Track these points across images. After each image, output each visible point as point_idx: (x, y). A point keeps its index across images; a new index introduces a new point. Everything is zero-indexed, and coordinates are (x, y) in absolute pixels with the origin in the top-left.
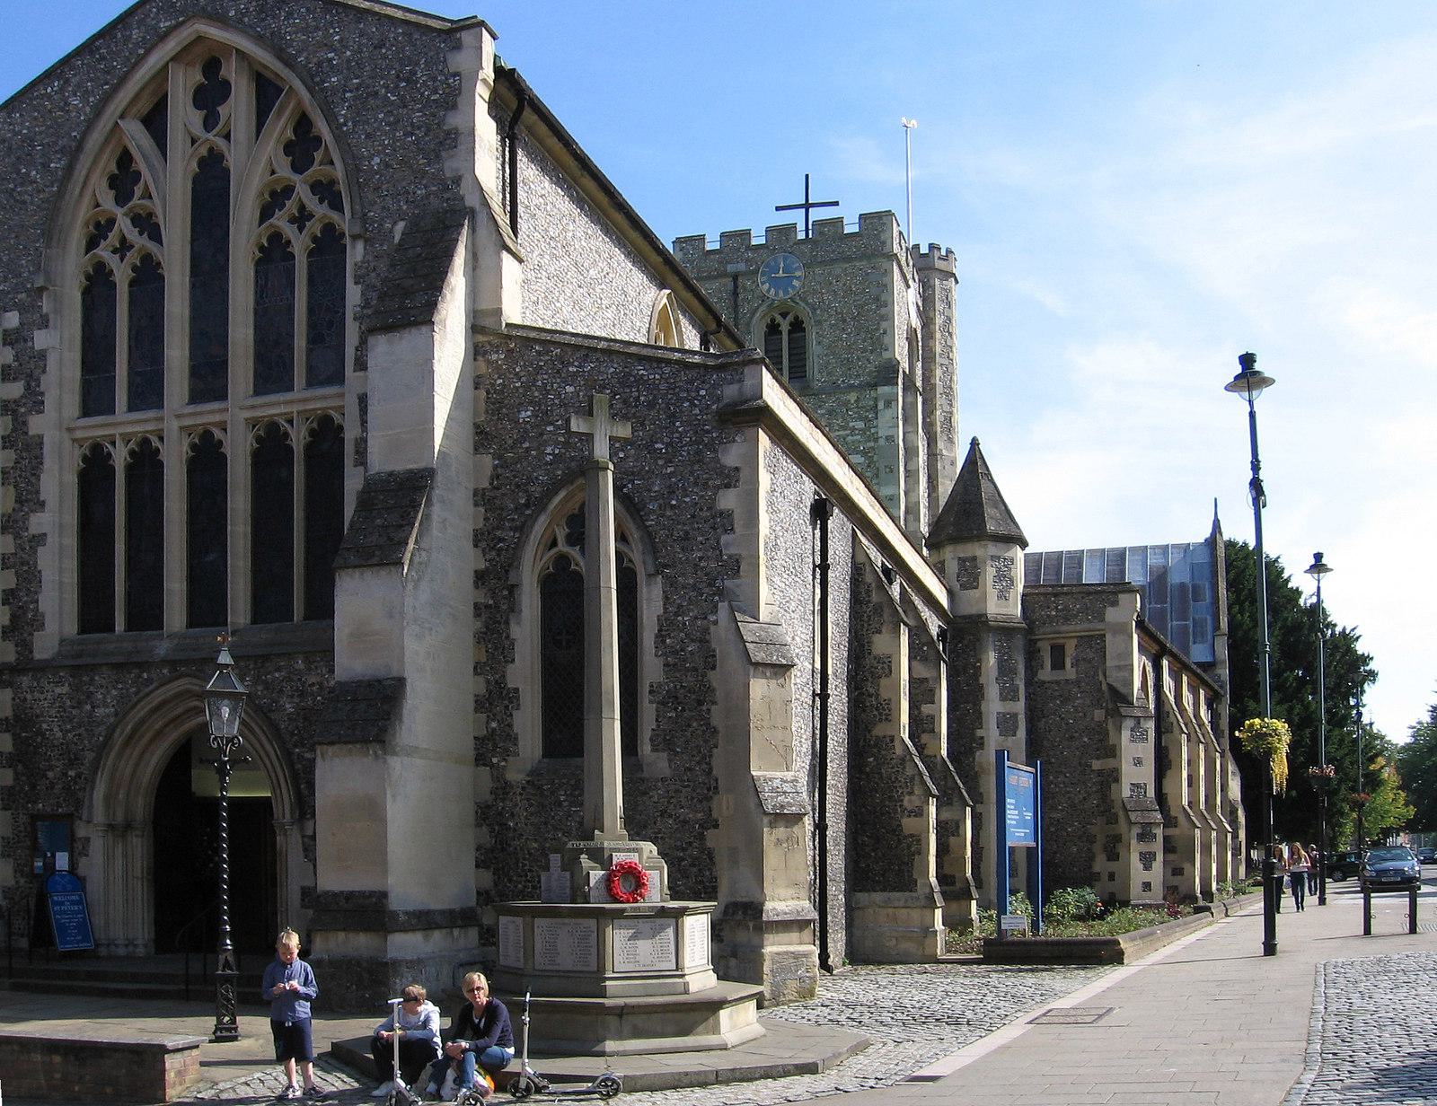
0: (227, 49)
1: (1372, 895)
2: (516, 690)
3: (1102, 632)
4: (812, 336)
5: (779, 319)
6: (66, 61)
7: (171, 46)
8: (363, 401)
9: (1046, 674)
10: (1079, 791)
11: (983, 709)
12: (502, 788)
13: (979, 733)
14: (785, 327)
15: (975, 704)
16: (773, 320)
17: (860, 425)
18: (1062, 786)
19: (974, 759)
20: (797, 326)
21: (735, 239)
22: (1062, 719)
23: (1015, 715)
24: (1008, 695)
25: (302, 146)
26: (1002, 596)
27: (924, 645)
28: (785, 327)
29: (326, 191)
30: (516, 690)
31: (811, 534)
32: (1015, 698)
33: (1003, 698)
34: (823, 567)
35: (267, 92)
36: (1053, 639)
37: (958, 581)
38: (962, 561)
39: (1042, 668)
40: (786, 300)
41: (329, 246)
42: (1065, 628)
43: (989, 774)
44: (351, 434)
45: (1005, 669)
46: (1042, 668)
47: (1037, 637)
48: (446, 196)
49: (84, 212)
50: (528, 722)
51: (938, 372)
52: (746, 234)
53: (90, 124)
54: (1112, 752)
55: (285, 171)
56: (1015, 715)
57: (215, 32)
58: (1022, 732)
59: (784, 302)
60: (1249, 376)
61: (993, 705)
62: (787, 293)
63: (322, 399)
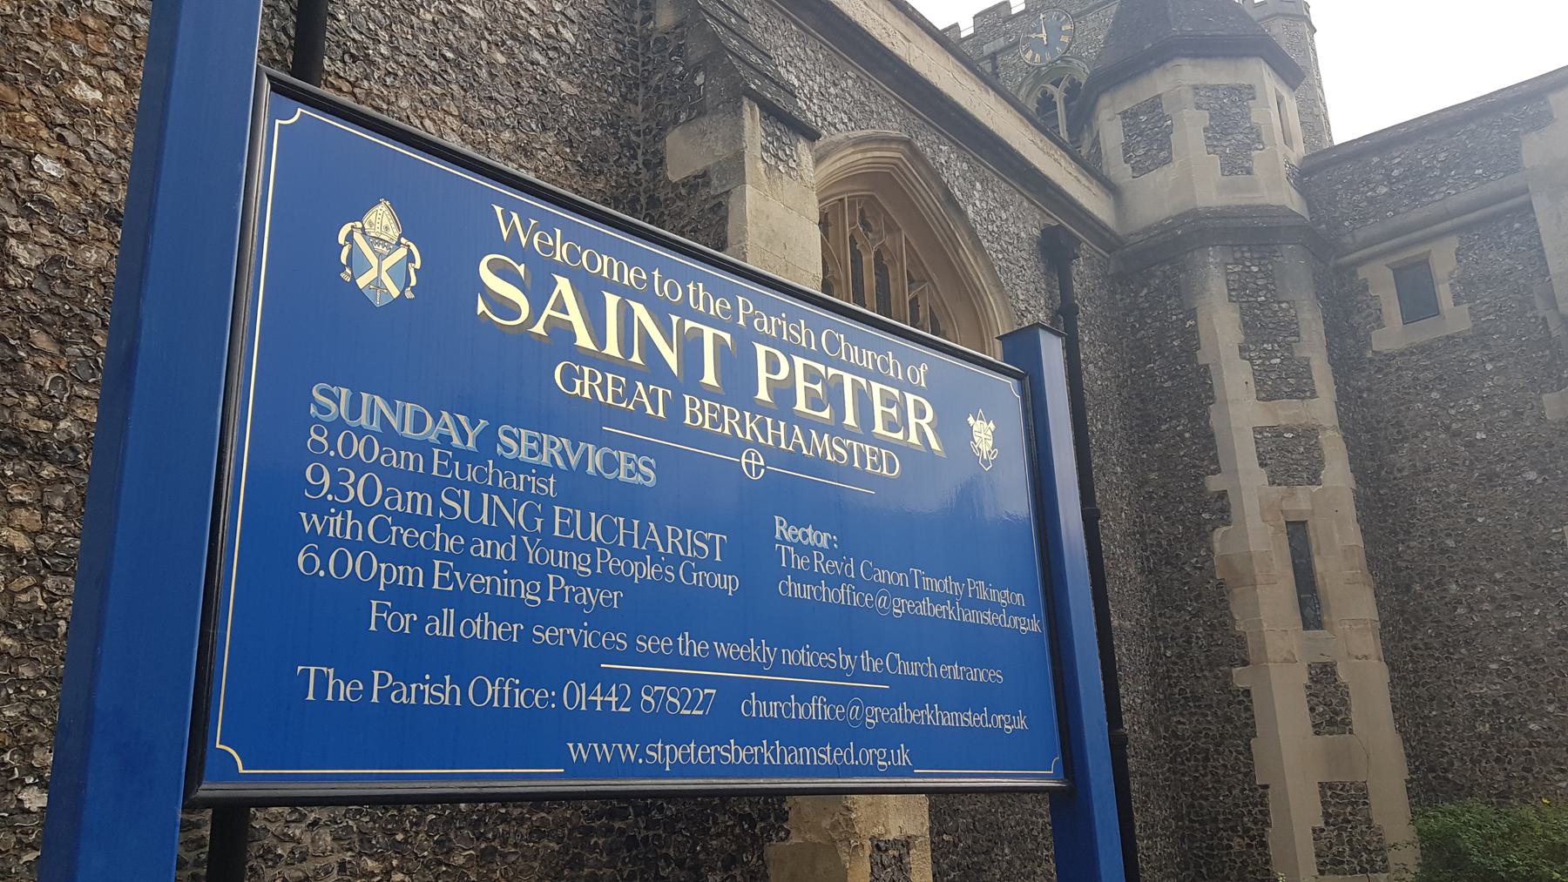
1: (452, 611)
2: (1247, 692)
3: (1522, 199)
5: (1051, 88)
10: (1542, 617)
11: (1215, 422)
13: (1214, 484)
16: (1044, 93)
18: (1486, 606)
19: (1210, 550)
22: (1456, 434)
23: (1309, 434)
30: (1247, 692)
32: (1303, 390)
33: (1267, 393)
36: (1393, 251)
38: (1129, 116)
39: (1381, 326)
43: (1254, 585)
46: (1381, 326)
56: (1309, 434)
58: (1338, 473)
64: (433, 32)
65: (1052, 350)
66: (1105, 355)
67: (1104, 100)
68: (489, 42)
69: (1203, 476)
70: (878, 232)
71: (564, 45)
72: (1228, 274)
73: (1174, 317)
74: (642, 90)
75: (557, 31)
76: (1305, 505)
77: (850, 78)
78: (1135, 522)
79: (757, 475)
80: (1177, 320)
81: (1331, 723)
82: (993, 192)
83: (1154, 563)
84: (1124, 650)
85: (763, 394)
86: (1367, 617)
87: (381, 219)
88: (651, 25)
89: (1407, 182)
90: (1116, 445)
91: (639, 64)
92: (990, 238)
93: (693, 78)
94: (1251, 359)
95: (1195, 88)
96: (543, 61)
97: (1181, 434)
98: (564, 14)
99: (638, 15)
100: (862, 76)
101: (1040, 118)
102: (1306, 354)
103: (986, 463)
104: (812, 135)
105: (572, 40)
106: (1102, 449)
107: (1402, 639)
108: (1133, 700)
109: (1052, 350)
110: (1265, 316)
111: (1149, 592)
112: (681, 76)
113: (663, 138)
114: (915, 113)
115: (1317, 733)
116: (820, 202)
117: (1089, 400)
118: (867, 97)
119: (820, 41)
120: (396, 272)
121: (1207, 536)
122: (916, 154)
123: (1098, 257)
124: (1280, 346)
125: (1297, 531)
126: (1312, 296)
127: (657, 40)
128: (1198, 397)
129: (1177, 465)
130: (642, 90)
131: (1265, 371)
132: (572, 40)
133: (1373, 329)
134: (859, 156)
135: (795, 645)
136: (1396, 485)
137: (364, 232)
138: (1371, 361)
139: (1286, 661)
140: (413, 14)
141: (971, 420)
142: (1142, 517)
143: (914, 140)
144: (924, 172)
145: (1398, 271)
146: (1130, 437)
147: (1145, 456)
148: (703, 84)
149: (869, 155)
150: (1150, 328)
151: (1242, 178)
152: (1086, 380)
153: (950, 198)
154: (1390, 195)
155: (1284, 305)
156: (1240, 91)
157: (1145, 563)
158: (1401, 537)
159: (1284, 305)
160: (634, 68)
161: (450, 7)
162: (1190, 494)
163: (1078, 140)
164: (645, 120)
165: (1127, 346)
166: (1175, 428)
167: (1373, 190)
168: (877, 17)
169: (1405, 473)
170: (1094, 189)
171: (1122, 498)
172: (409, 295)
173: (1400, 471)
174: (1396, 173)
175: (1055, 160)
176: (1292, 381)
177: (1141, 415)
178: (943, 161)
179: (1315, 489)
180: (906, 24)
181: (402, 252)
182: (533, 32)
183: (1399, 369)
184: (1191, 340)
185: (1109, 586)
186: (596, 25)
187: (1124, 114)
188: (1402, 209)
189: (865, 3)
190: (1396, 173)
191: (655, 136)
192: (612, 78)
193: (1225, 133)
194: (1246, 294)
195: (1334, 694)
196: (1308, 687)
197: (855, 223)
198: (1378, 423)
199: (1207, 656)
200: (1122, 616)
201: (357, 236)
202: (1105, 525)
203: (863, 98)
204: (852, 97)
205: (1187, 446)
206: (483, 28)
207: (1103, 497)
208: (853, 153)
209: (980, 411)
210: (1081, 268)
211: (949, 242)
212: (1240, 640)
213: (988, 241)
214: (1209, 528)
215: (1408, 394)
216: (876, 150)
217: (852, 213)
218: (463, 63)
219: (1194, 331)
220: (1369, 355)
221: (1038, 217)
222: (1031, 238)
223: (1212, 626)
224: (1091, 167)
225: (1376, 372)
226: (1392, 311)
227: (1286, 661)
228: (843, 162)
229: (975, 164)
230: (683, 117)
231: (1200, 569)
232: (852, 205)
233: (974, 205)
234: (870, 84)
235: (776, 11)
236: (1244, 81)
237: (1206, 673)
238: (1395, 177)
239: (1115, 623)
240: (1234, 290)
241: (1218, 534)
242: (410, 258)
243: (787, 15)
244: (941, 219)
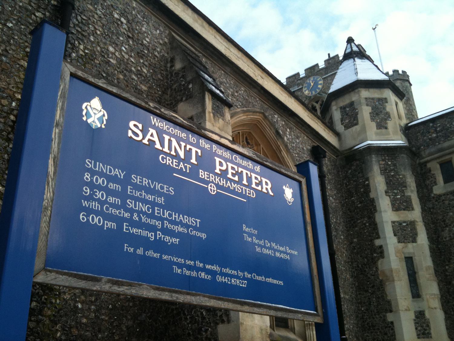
2: (392, 323)
5: (315, 104)
11: (377, 220)
13: (377, 242)
15: (369, 218)
19: (377, 268)
26: (382, 125)
27: (189, 83)
30: (392, 323)
32: (409, 207)
33: (396, 207)
37: (342, 124)
40: (316, 95)
42: (446, 144)
43: (393, 281)
47: (426, 159)
48: (177, 90)
52: (298, 74)
56: (412, 224)
58: (423, 238)
59: (315, 96)
62: (316, 91)
64: (99, 67)
65: (314, 170)
66: (336, 194)
67: (333, 103)
68: (118, 71)
69: (374, 240)
70: (252, 145)
71: (143, 73)
72: (380, 165)
73: (361, 181)
74: (170, 90)
75: (141, 69)
76: (411, 251)
77: (242, 90)
78: (349, 258)
79: (214, 192)
80: (362, 181)
81: (423, 334)
82: (294, 133)
83: (357, 274)
84: (346, 307)
85: (217, 171)
86: (436, 293)
87: (96, 103)
88: (174, 68)
89: (443, 133)
90: (341, 228)
91: (169, 81)
92: (293, 149)
93: (188, 85)
94: (389, 196)
95: (366, 98)
96: (136, 79)
97: (365, 224)
98: (143, 64)
99: (169, 65)
100: (247, 90)
101: (312, 110)
102: (409, 194)
103: (290, 202)
104: (229, 106)
105: (146, 72)
106: (336, 229)
107: (448, 302)
108: (350, 326)
109: (314, 170)
110: (394, 180)
111: (355, 285)
112: (184, 85)
113: (177, 106)
114: (265, 103)
115: (419, 338)
116: (232, 132)
117: (330, 210)
118: (248, 97)
119: (232, 77)
120: (100, 119)
121: (376, 263)
122: (265, 117)
123: (332, 158)
124: (400, 191)
125: (409, 261)
126: (411, 173)
127: (175, 73)
128: (371, 210)
129: (364, 236)
130: (170, 90)
131: (395, 200)
132: (146, 72)
133: (433, 186)
134: (245, 117)
135: (226, 268)
136: (444, 244)
137: (90, 106)
138: (433, 198)
139: (406, 310)
140: (93, 61)
141: (284, 187)
142: (351, 256)
143: (265, 113)
144: (269, 124)
145: (442, 165)
146: (346, 225)
147: (352, 232)
148: (192, 88)
149: (249, 117)
150: (352, 184)
151: (384, 130)
152: (329, 202)
153: (277, 133)
154: (437, 137)
155: (401, 176)
156: (382, 100)
157: (353, 274)
158: (447, 263)
159: (401, 176)
160: (167, 82)
161: (105, 59)
162: (369, 247)
163: (324, 118)
164: (170, 100)
165: (344, 191)
166: (363, 222)
167: (431, 135)
168: (252, 70)
169: (448, 239)
170: (331, 134)
171: (344, 248)
172: (103, 127)
173: (445, 238)
174: (438, 129)
175: (316, 123)
176: (405, 204)
177: (350, 217)
178: (276, 121)
179: (414, 244)
180: (262, 73)
181: (101, 113)
182: (133, 69)
183: (443, 200)
184: (367, 189)
185: (340, 282)
186: (154, 68)
187: (341, 108)
188: (441, 142)
189: (248, 65)
190: (438, 129)
191: (174, 105)
192: (159, 85)
193: (377, 114)
194: (386, 172)
195: (424, 323)
196: (415, 320)
197: (244, 141)
198: (437, 220)
199: (377, 310)
200: (345, 293)
201: (89, 107)
202: (338, 258)
203: (247, 98)
204: (243, 97)
205: (367, 229)
206: (116, 66)
207: (336, 247)
208: (243, 116)
209: (287, 185)
210: (326, 162)
211: (278, 149)
212: (389, 302)
213: (292, 150)
214: (376, 259)
215: (447, 209)
216: (252, 115)
217: (243, 138)
218: (109, 78)
219: (368, 185)
220: (433, 195)
221: (310, 142)
222: (308, 149)
223: (379, 298)
224: (330, 126)
225: (435, 201)
226: (440, 179)
227: (406, 310)
228: (240, 119)
229: (287, 122)
230: (184, 99)
231: (374, 275)
232: (243, 135)
233: (287, 137)
234: (249, 93)
235: (217, 67)
236: (384, 96)
237: (377, 316)
238: (438, 131)
239: (342, 296)
240: (382, 170)
241: (379, 262)
242: (104, 115)
243: (220, 68)
244: (275, 141)
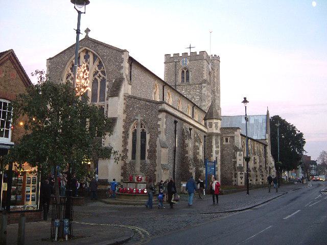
0: (90, 51)
4: (190, 73)
6: (65, 51)
7: (81, 50)
8: (108, 105)
9: (224, 143)
12: (125, 164)
14: (185, 71)
17: (199, 91)
20: (187, 71)
21: (176, 55)
24: (217, 147)
25: (100, 65)
28: (185, 71)
29: (103, 72)
31: (174, 125)
34: (175, 131)
35: (95, 57)
41: (103, 81)
44: (105, 110)
45: (217, 143)
49: (66, 73)
50: (129, 154)
51: (216, 79)
53: (68, 61)
54: (235, 158)
55: (97, 69)
57: (88, 49)
58: (220, 154)
60: (245, 101)
61: (214, 149)
63: (101, 104)
